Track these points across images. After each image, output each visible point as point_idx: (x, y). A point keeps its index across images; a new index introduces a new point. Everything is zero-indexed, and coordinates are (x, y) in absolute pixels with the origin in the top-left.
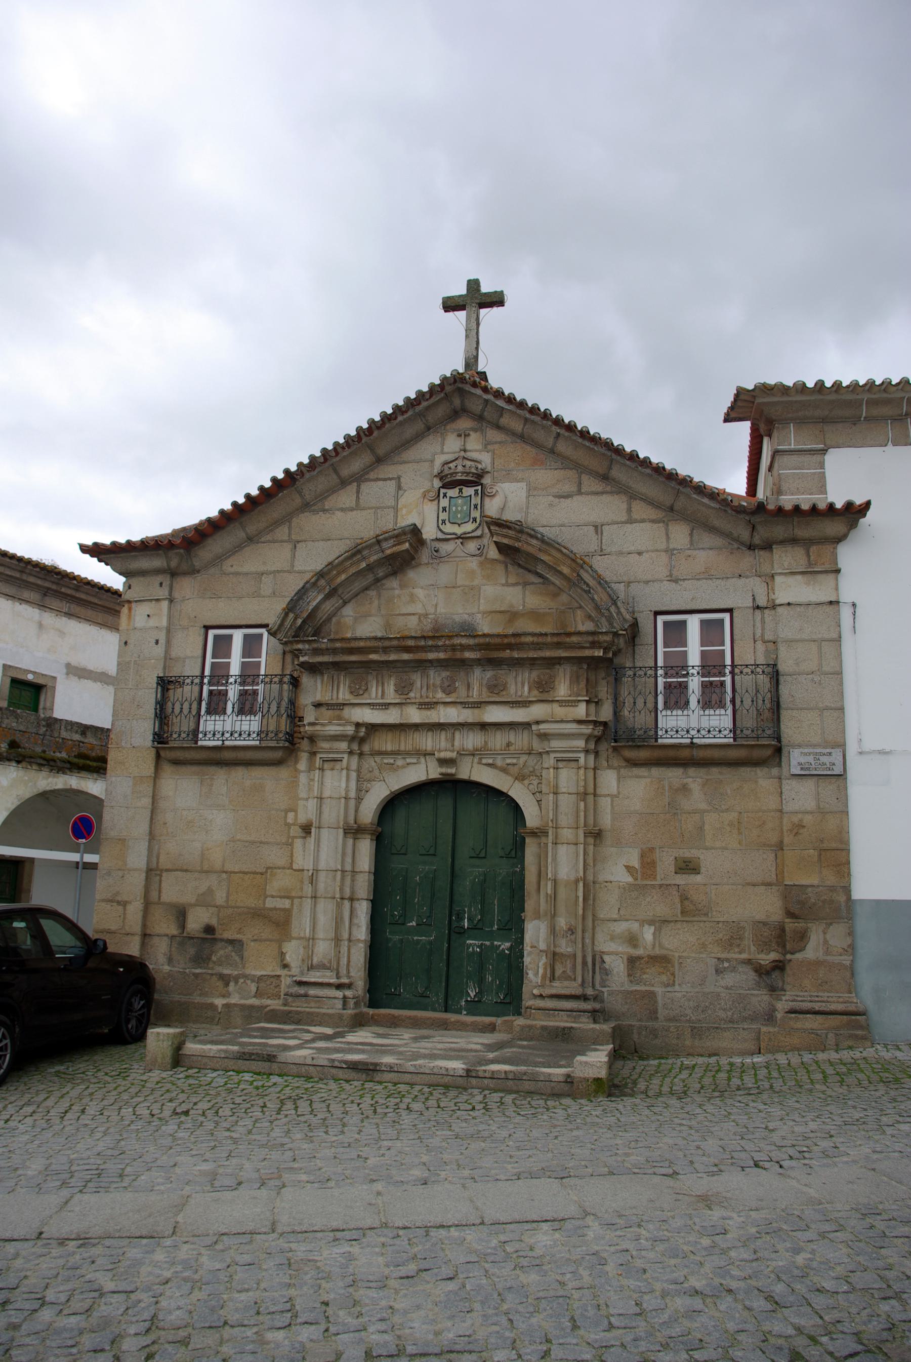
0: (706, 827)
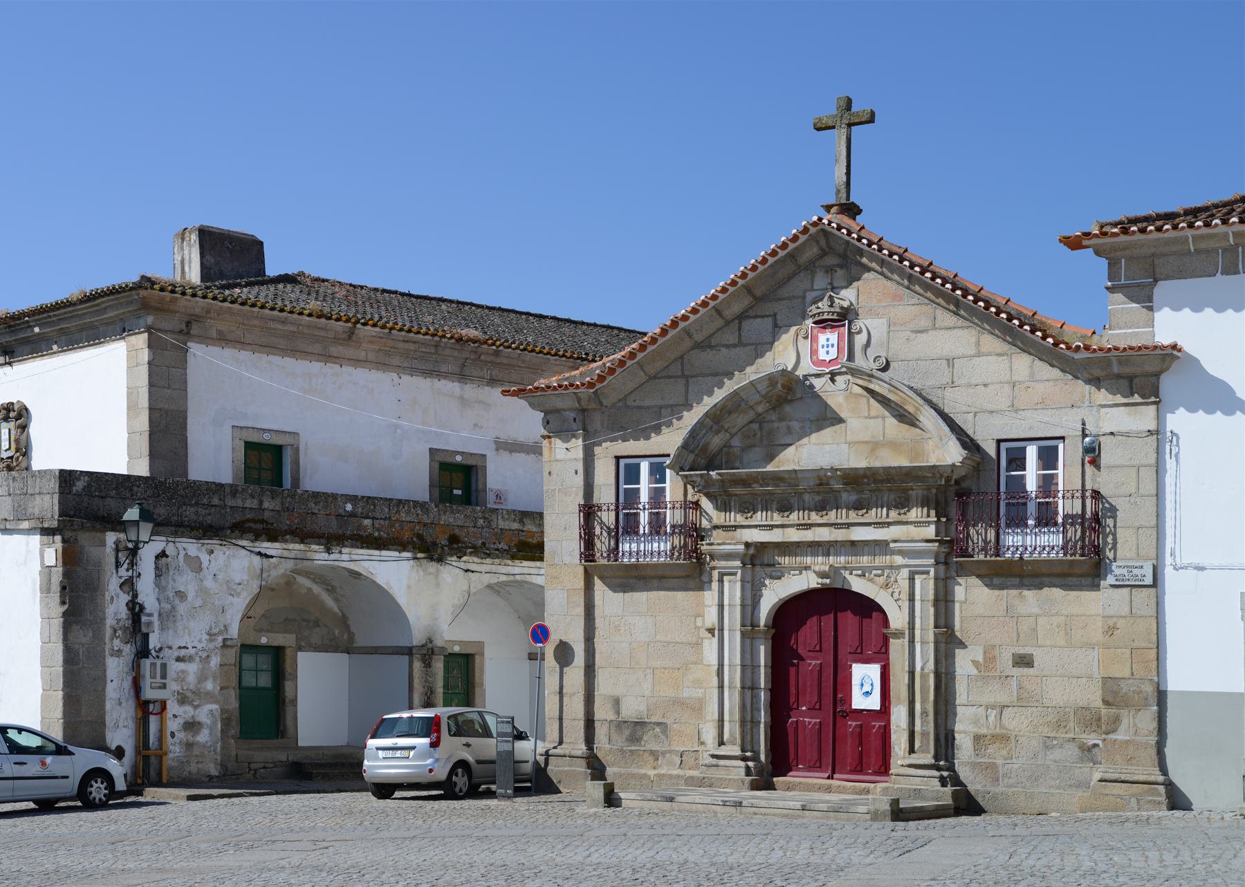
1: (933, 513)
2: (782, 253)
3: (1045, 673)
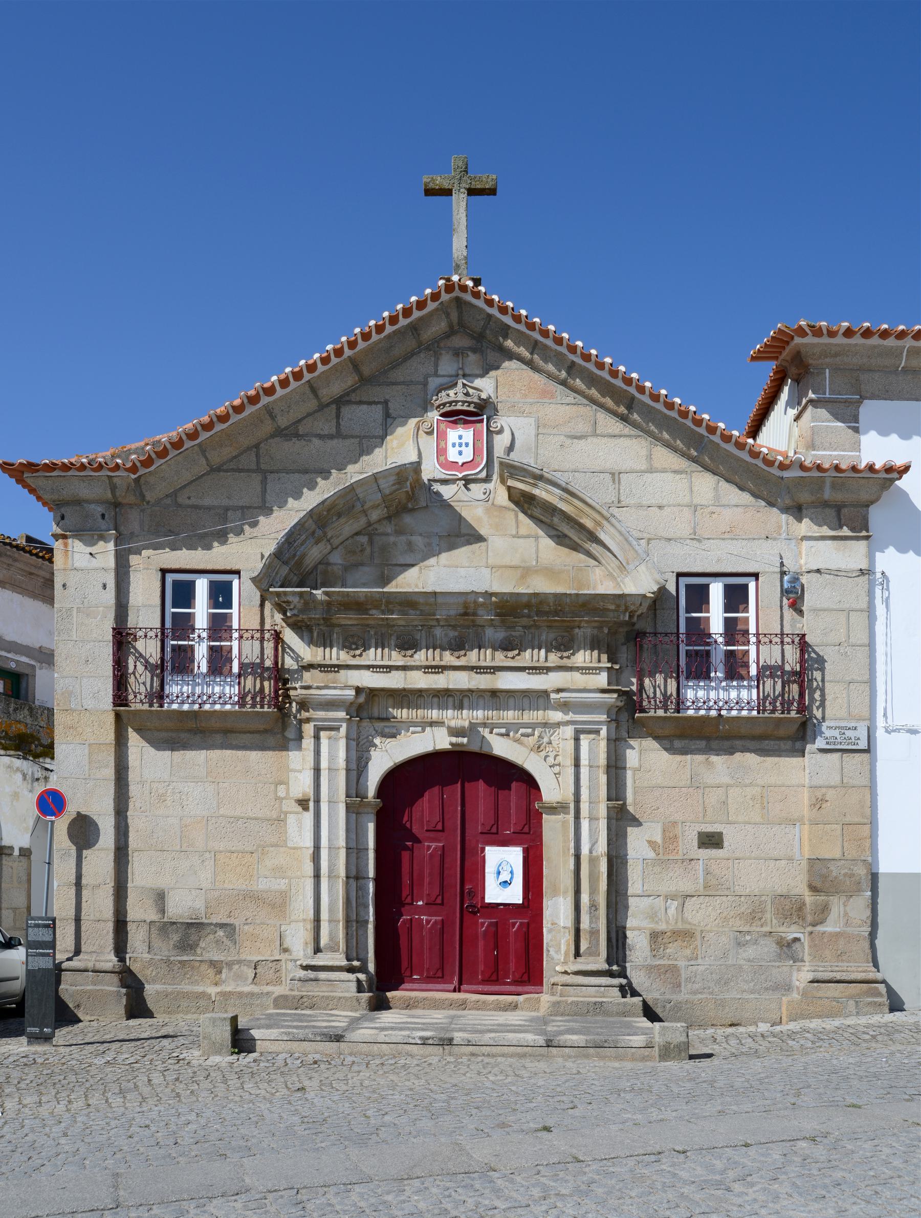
0: (730, 801)
1: (604, 657)
2: (403, 322)
3: (737, 855)
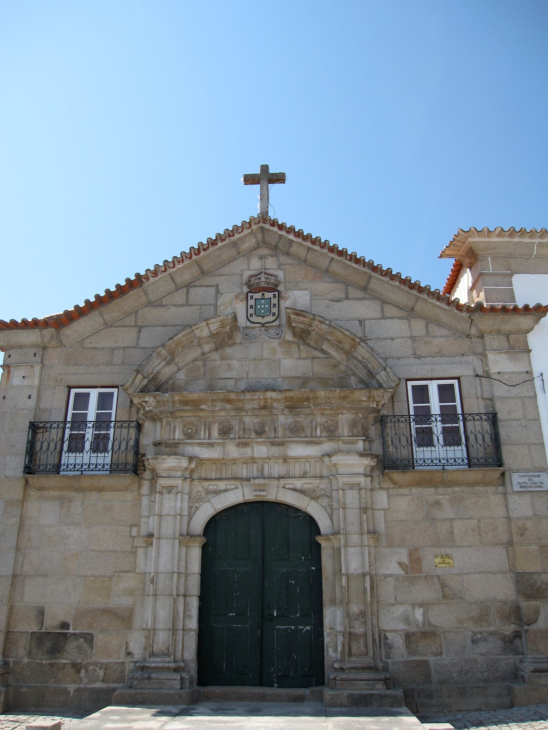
0: (455, 531)
